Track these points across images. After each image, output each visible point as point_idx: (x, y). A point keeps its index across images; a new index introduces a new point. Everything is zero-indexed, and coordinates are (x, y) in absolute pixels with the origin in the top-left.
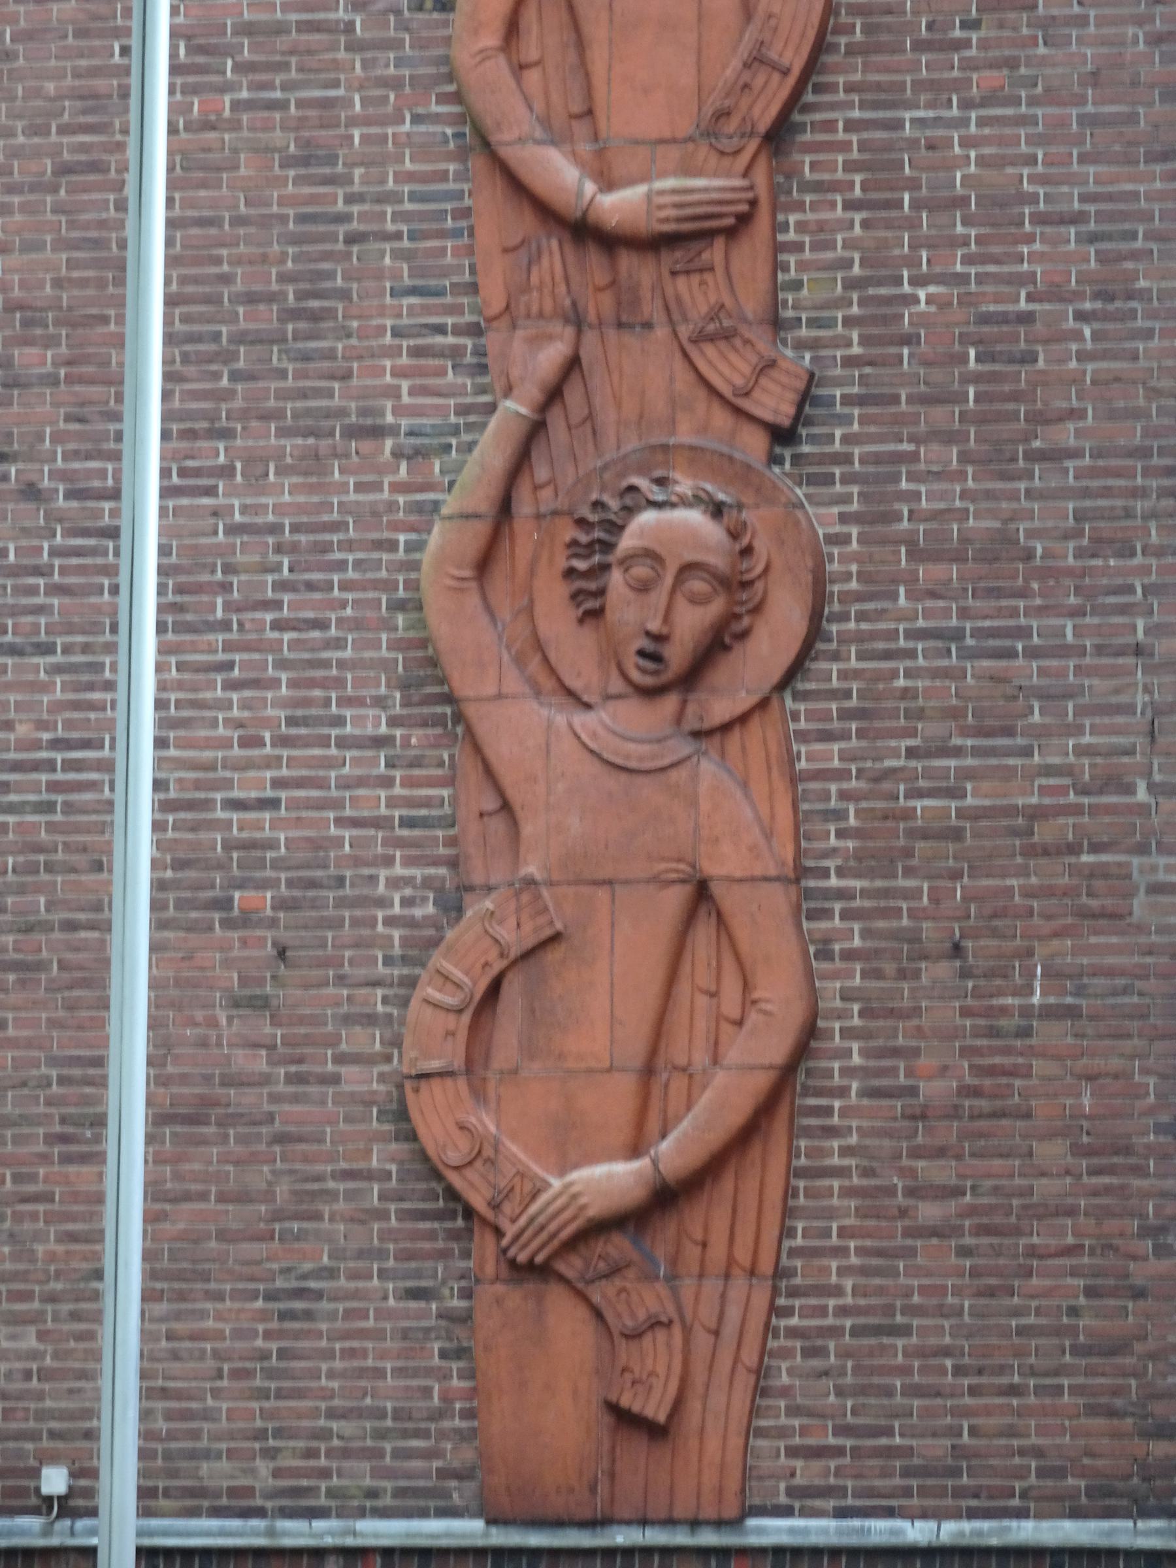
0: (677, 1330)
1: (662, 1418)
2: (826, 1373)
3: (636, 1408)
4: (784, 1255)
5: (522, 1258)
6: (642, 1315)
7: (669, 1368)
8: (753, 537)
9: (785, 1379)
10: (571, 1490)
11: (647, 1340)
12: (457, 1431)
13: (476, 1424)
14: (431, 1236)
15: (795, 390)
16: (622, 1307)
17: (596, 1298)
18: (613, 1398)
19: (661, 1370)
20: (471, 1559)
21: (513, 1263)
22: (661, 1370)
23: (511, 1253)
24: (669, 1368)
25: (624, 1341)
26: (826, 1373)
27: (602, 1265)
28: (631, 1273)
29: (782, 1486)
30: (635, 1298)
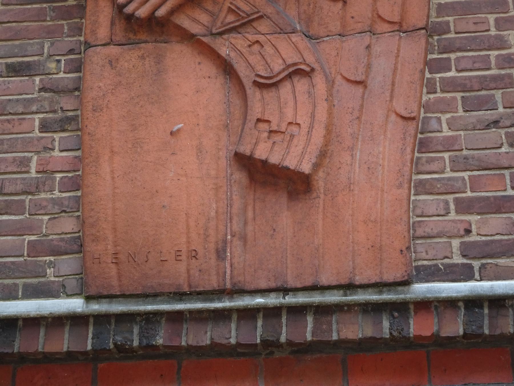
0: (319, 80)
1: (306, 168)
2: (496, 123)
3: (274, 159)
4: (433, 13)
5: (143, 12)
6: (277, 66)
7: (313, 116)
8: (266, 19)
9: (447, 132)
10: (194, 255)
11: (286, 89)
12: (54, 201)
13: (79, 193)
14: (40, 16)
15: (261, 93)
16: (254, 59)
17: (224, 51)
18: (246, 149)
19: (303, 120)
20: (67, 329)
21: (130, 18)
22: (303, 120)
23: (129, 9)
24: (313, 116)
25: (258, 94)
26: (496, 123)
27: (231, 18)
28: (263, 26)
29: (456, 243)
30: (269, 50)
